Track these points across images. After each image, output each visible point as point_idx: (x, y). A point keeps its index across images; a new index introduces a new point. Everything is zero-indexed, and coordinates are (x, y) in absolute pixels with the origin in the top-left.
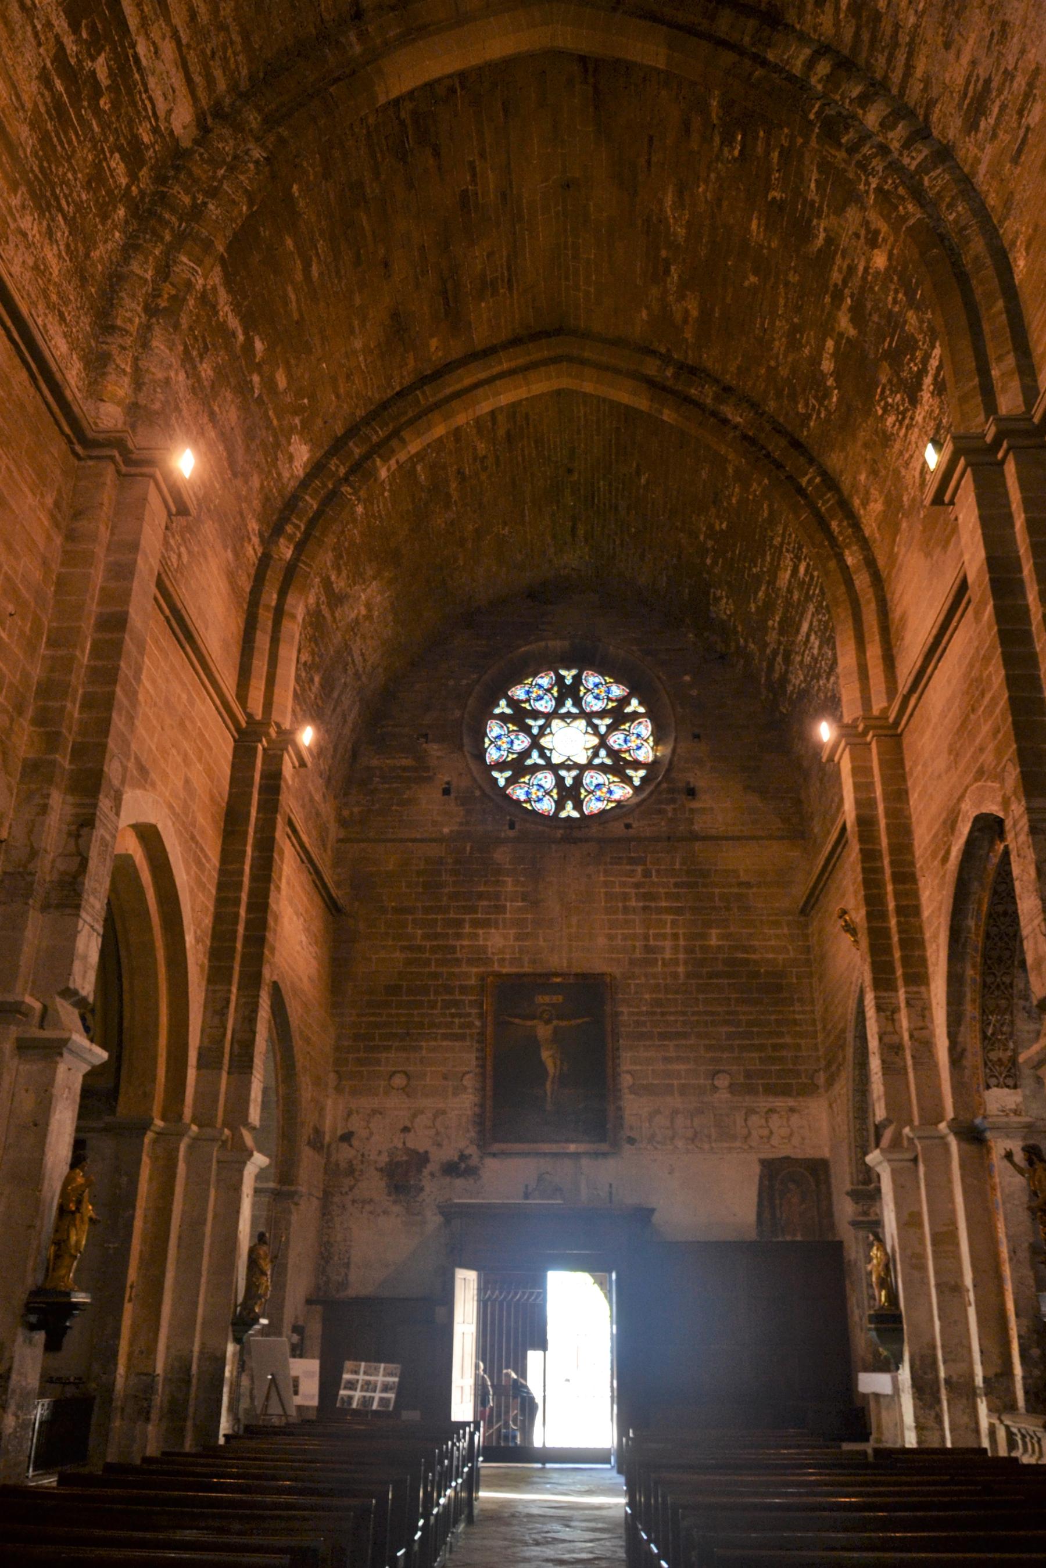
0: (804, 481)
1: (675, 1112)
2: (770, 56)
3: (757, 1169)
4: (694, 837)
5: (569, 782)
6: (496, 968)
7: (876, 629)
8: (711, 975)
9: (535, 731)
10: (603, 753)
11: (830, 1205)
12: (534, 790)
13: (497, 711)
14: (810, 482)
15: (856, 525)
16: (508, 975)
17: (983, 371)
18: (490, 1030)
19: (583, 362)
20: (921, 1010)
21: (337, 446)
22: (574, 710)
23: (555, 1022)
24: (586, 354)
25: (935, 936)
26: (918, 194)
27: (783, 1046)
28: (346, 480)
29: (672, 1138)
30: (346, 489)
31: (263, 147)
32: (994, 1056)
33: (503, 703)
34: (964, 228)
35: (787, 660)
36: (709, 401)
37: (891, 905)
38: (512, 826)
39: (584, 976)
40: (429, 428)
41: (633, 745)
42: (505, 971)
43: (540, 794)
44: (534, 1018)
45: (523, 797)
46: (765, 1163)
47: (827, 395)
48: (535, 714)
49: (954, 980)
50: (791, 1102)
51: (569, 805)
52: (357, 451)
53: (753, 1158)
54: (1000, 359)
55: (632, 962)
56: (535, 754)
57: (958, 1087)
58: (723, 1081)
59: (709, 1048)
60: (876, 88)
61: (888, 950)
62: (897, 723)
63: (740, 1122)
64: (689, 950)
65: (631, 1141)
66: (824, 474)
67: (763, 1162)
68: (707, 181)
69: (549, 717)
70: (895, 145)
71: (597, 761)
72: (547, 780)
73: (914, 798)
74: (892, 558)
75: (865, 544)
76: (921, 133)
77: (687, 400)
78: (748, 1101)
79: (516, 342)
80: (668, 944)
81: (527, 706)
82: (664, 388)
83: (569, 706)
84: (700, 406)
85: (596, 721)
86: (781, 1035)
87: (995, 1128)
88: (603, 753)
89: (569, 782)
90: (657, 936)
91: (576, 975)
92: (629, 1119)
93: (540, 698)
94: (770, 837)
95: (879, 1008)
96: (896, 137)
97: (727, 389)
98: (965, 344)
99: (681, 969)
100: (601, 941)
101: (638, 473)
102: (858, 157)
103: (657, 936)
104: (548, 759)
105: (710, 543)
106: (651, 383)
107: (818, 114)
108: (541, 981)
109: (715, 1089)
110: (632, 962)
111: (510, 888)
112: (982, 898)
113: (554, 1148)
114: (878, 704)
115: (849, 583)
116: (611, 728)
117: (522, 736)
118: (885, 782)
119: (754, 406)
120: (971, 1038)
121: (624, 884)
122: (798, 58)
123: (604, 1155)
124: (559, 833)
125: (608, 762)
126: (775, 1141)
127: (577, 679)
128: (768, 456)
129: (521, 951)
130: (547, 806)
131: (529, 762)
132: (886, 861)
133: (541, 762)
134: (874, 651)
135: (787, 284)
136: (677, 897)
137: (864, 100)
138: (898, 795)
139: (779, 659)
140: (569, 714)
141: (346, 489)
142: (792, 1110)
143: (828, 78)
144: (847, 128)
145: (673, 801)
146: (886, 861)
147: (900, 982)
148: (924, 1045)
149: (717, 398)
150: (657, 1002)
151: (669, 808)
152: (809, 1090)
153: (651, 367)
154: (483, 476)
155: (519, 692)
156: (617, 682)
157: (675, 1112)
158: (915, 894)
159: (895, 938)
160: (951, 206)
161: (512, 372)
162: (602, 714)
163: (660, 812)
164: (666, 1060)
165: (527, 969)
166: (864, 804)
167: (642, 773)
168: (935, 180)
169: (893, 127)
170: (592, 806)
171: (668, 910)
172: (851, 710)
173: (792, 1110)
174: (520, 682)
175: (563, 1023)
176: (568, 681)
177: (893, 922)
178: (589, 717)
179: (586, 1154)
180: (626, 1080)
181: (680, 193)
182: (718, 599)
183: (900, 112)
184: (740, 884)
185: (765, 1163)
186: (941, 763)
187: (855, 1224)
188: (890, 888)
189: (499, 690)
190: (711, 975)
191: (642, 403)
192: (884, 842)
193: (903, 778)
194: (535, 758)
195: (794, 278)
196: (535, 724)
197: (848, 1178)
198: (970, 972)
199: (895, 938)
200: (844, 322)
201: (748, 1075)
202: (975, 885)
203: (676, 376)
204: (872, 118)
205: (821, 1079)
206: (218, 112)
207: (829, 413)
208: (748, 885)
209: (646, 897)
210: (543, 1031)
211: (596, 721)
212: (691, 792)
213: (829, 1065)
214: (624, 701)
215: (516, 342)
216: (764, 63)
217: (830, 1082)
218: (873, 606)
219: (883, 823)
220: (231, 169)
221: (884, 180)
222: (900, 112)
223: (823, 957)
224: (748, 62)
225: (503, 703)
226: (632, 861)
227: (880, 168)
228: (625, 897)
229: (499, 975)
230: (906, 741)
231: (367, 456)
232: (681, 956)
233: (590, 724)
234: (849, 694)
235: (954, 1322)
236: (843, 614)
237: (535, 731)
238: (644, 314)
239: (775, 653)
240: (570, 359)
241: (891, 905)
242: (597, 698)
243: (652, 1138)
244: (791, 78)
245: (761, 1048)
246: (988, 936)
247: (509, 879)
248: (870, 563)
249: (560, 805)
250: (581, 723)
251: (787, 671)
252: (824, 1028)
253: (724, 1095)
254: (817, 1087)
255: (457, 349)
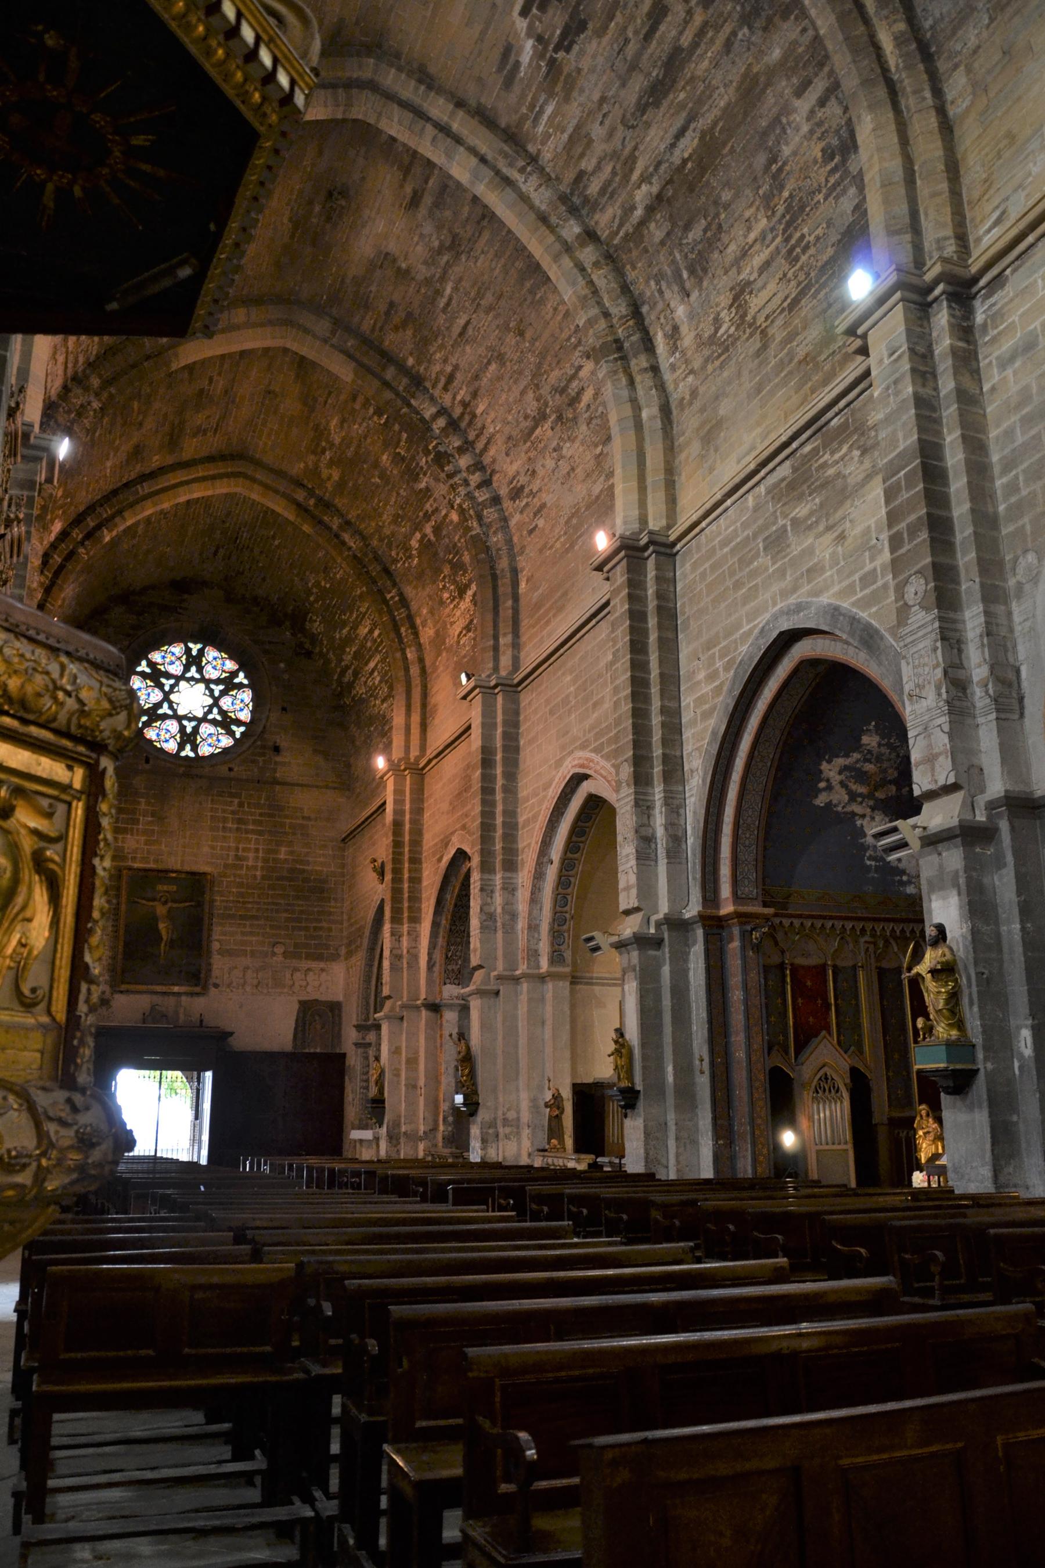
0: (388, 596)
1: (247, 968)
2: (413, 402)
3: (296, 1006)
4: (276, 782)
5: (189, 730)
6: (130, 863)
7: (418, 705)
8: (278, 879)
9: (167, 688)
10: (215, 710)
11: (340, 1029)
12: (163, 733)
13: (139, 669)
14: (392, 598)
15: (416, 634)
16: (140, 870)
17: (496, 638)
18: (123, 907)
19: (254, 480)
20: (414, 935)
21: (78, 520)
22: (197, 676)
23: (169, 904)
24: (258, 476)
25: (429, 899)
26: (480, 518)
27: (321, 928)
28: (82, 543)
29: (243, 986)
30: (81, 550)
31: (99, 400)
32: (450, 967)
33: (144, 663)
34: (499, 549)
35: (356, 674)
36: (335, 527)
37: (406, 876)
38: (147, 761)
39: (193, 874)
40: (143, 510)
41: (237, 707)
42: (136, 865)
43: (167, 736)
44: (154, 900)
45: (154, 738)
46: (302, 1003)
47: (410, 557)
48: (168, 675)
49: (435, 925)
50: (322, 965)
51: (188, 747)
52: (92, 524)
53: (295, 999)
54: (505, 635)
55: (226, 866)
56: (166, 705)
57: (430, 982)
58: (279, 950)
59: (272, 927)
60: (467, 447)
61: (401, 901)
62: (423, 768)
63: (288, 976)
64: (265, 860)
65: (216, 986)
66: (401, 594)
67: (300, 1002)
68: (360, 425)
69: (178, 679)
70: (473, 484)
71: (210, 717)
72: (173, 726)
73: (427, 815)
74: (435, 669)
75: (419, 647)
76: (486, 483)
77: (321, 522)
78: (295, 963)
79: (210, 459)
80: (251, 855)
81: (162, 668)
82: (306, 510)
83: (193, 672)
84: (329, 528)
85: (212, 686)
86: (320, 921)
87: (446, 1005)
88: (215, 710)
89: (189, 730)
90: (244, 850)
91: (187, 873)
92: (216, 972)
93: (172, 663)
94: (327, 787)
95: (392, 934)
96: (475, 479)
97: (348, 523)
98: (489, 617)
99: (258, 873)
100: (206, 849)
101: (274, 538)
102: (452, 481)
103: (244, 850)
104: (175, 711)
105: (315, 590)
106: (299, 505)
107: (435, 447)
108: (162, 875)
109: (274, 954)
110: (226, 866)
111: (143, 806)
112: (456, 884)
113: (164, 989)
114: (414, 753)
115: (407, 670)
116: (224, 693)
117: (157, 690)
118: (412, 801)
119: (364, 538)
120: (438, 956)
121: (224, 811)
122: (429, 412)
123: (198, 994)
124: (181, 770)
125: (219, 718)
126: (309, 989)
127: (201, 652)
128: (367, 572)
129: (149, 852)
130: (171, 746)
131: (160, 711)
132: (407, 849)
133: (170, 712)
134: (416, 718)
135: (398, 494)
136: (260, 823)
137: (461, 450)
138: (418, 811)
139: (350, 671)
140: (192, 679)
141: (81, 550)
142: (322, 970)
143: (443, 430)
144: (449, 462)
145: (263, 755)
146: (407, 849)
147: (405, 920)
148: (414, 957)
149: (340, 527)
150: (242, 895)
151: (261, 759)
152: (334, 957)
153: (300, 495)
154: (163, 522)
155: (156, 656)
156: (231, 658)
157: (247, 968)
158: (419, 871)
159: (406, 895)
160: (495, 533)
161: (204, 479)
162: (218, 681)
163: (253, 761)
164: (243, 934)
165: (152, 866)
166: (398, 812)
167: (242, 729)
168: (490, 514)
169: (473, 473)
170: (205, 750)
171: (253, 832)
172: (397, 753)
173: (322, 970)
174: (158, 649)
175: (175, 905)
176: (194, 653)
177: (406, 885)
178: (207, 682)
179: (186, 994)
180: (216, 946)
181: (343, 421)
182: (312, 621)
183: (478, 466)
184: (303, 818)
185: (302, 1003)
186: (445, 806)
187: (356, 1044)
188: (406, 865)
189: (142, 653)
190: (278, 879)
191: (289, 514)
192: (407, 838)
193: (422, 801)
194: (165, 709)
195: (402, 493)
196: (167, 683)
197: (354, 1016)
198: (444, 922)
199: (406, 895)
200: (428, 529)
201: (296, 946)
202: (453, 879)
203: (316, 505)
204: (464, 462)
205: (343, 951)
206: (75, 378)
207: (410, 567)
208: (309, 818)
209: (240, 821)
210: (161, 910)
211: (212, 686)
212: (277, 749)
213: (349, 944)
214: (234, 674)
215: (210, 459)
216: (409, 405)
217: (350, 954)
218: (419, 689)
219: (407, 827)
220: (79, 415)
221: (464, 501)
222: (478, 466)
223: (353, 876)
224: (399, 402)
225: (144, 663)
226: (232, 795)
227: (463, 493)
228: (225, 820)
229: (130, 869)
230: (427, 780)
231: (99, 527)
232: (260, 864)
233: (208, 688)
234: (398, 740)
235: (411, 1104)
236: (400, 689)
237: (167, 688)
238: (302, 465)
239: (347, 667)
240: (246, 476)
241: (406, 876)
242: (214, 668)
243: (229, 985)
244: (423, 420)
245: (307, 929)
246: (456, 905)
247: (143, 800)
248: (421, 660)
249: (181, 747)
250: (201, 686)
251: (354, 682)
252: (349, 919)
253: (280, 958)
254: (339, 955)
255: (170, 460)
